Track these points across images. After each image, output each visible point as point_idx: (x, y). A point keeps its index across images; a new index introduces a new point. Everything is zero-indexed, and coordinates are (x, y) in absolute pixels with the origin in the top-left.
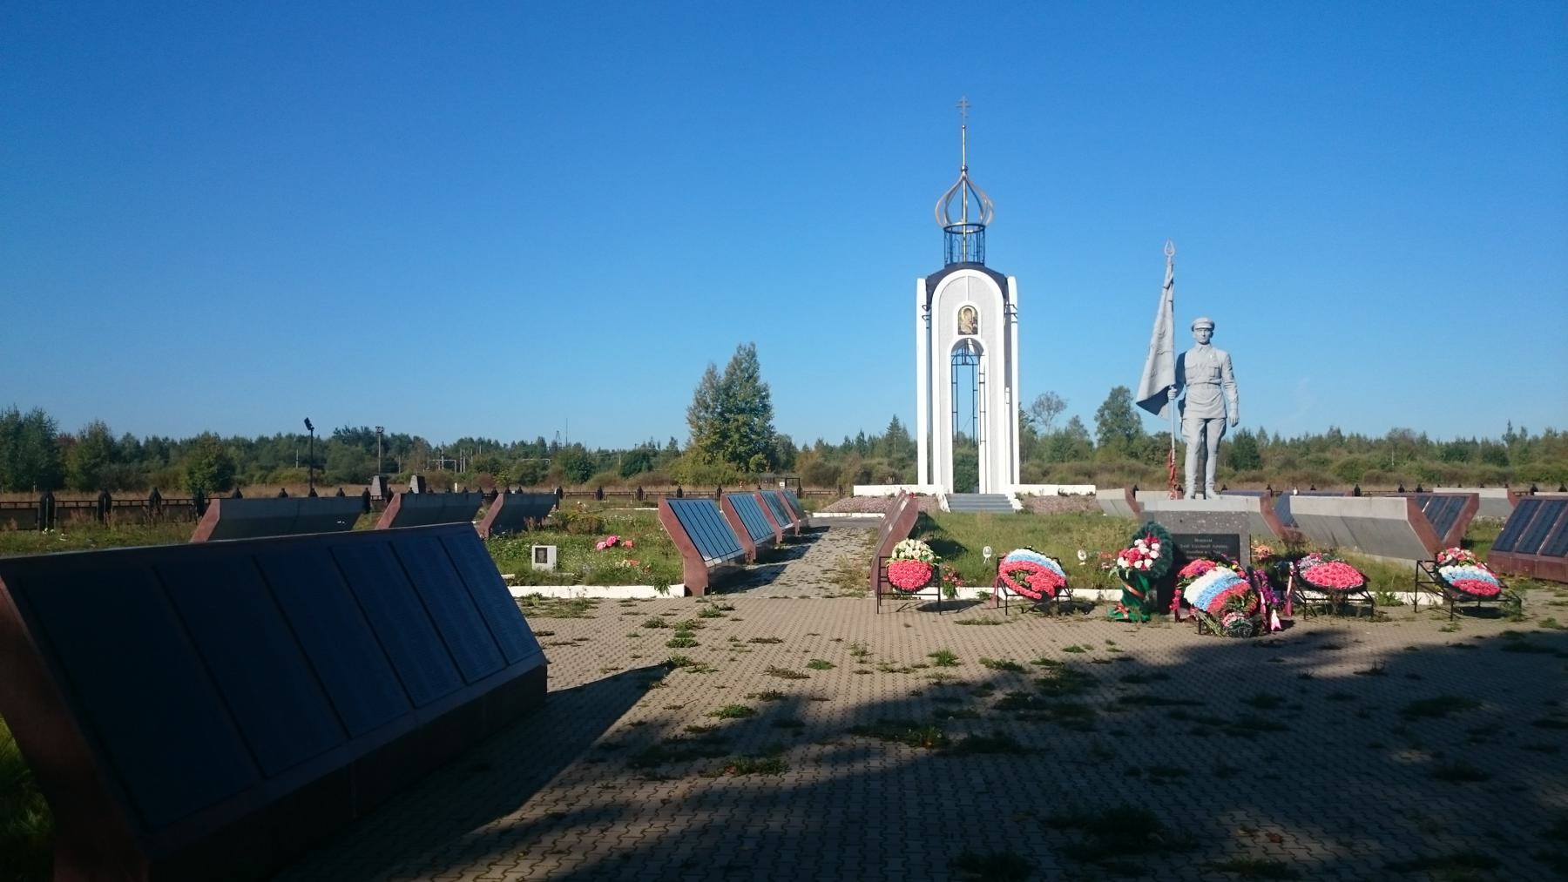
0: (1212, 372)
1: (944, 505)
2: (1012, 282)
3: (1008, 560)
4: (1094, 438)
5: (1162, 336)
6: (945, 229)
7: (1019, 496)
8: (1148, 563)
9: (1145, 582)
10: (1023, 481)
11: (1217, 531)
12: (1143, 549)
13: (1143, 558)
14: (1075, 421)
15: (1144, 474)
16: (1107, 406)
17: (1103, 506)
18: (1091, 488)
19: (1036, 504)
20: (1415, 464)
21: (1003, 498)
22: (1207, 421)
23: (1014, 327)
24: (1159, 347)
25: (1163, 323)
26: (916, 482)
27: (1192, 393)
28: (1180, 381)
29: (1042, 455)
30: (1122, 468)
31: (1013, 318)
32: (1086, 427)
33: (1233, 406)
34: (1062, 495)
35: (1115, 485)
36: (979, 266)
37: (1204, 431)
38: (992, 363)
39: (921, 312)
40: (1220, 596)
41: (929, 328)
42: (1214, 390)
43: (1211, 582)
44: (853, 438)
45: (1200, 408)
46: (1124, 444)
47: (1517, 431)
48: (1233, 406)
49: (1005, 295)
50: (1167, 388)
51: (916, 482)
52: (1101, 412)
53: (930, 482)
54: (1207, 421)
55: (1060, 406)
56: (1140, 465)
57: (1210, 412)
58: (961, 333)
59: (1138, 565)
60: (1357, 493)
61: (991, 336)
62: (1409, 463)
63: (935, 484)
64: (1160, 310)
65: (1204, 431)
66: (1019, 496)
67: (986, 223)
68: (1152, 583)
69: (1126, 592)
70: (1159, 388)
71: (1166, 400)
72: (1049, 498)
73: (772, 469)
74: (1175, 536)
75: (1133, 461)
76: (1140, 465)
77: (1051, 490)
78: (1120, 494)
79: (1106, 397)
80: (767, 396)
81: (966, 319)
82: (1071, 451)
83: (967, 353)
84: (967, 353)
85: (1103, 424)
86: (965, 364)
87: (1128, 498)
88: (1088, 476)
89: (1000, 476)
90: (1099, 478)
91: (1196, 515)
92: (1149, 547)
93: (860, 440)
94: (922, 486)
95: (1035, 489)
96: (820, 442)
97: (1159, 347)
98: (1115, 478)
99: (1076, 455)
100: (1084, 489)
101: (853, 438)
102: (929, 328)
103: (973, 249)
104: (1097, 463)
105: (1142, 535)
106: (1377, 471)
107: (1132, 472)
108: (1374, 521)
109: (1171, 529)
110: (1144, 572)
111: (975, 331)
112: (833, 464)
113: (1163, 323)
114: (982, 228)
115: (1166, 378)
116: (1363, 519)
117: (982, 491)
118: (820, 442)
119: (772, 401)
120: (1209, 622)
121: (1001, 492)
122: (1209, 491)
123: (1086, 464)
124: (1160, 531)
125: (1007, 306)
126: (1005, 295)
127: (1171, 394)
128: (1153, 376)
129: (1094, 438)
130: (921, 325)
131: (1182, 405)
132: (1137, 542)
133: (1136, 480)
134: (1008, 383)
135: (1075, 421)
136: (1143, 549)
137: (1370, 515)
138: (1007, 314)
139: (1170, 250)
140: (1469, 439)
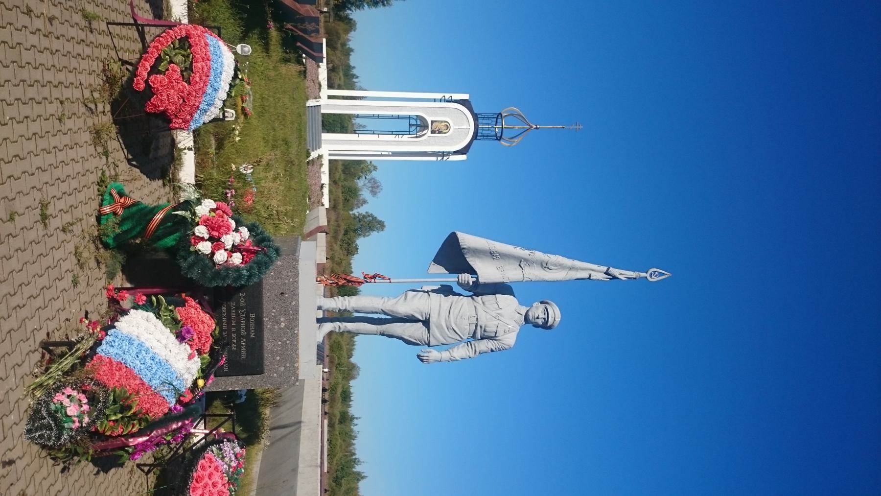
0: (491, 329)
1: (311, 103)
2: (463, 157)
3: (212, 40)
4: (355, 212)
5: (544, 265)
6: (500, 114)
7: (320, 157)
8: (205, 247)
9: (170, 241)
10: (330, 161)
11: (268, 345)
12: (229, 240)
13: (211, 239)
14: (365, 202)
15: (335, 238)
16: (375, 218)
17: (314, 211)
18: (327, 205)
19: (315, 168)
20: (340, 380)
21: (320, 147)
22: (426, 323)
23: (434, 159)
24: (529, 262)
25: (562, 267)
26: (330, 86)
27: (464, 305)
28: (479, 289)
29: (347, 172)
30: (339, 226)
31: (440, 158)
32: (362, 208)
33: (445, 355)
34: (322, 186)
35: (329, 222)
36: (475, 136)
37: (412, 319)
38: (407, 143)
39: (447, 96)
40: (130, 374)
41: (435, 100)
42: (466, 329)
43: (162, 353)
44: (354, 72)
45: (444, 313)
46: (352, 227)
47: (355, 421)
48: (445, 355)
49: (456, 153)
50: (472, 271)
51: (330, 86)
52: (371, 215)
53: (330, 97)
54: (426, 323)
55: (374, 193)
56: (340, 236)
57: (439, 327)
58: (432, 122)
59: (201, 231)
60: (324, 390)
61: (428, 143)
62: (341, 377)
63: (327, 101)
64: (578, 263)
65: (412, 319)
66: (320, 157)
67: (502, 142)
68: (172, 251)
69: (153, 211)
70: (475, 263)
71: (451, 270)
72: (319, 178)
73: (336, 5)
74: (259, 285)
75: (343, 232)
76: (340, 236)
77: (325, 179)
78: (323, 221)
79: (379, 218)
80: (384, 5)
81: (442, 126)
82: (348, 198)
83: (419, 125)
84: (419, 125)
85: (364, 216)
86: (411, 125)
87: (321, 227)
88: (334, 207)
89: (331, 146)
90: (333, 213)
91: (292, 316)
92: (235, 249)
93: (353, 76)
94: (325, 92)
95: (325, 168)
96: (352, 50)
97: (529, 262)
98: (332, 222)
99: (346, 200)
100: (326, 200)
101: (354, 72)
102: (435, 100)
103: (485, 133)
104: (342, 212)
105: (260, 238)
106: (336, 361)
107: (336, 232)
108: (295, 470)
109: (270, 280)
110: (187, 241)
111: (433, 132)
112: (339, 46)
113: (562, 267)
114: (499, 138)
115: (487, 271)
116: (297, 455)
117: (325, 136)
118: (352, 50)
119: (381, 8)
120: (68, 362)
121: (323, 146)
122: (328, 327)
123: (341, 206)
124: (263, 266)
125: (449, 154)
126: (456, 153)
127: (466, 277)
128: (492, 255)
129: (355, 212)
130: (439, 96)
131: (446, 290)
132: (244, 231)
133: (331, 234)
134: (395, 154)
135: (365, 202)
136: (229, 240)
137: (301, 466)
138: (443, 154)
139: (654, 275)
140: (352, 398)
